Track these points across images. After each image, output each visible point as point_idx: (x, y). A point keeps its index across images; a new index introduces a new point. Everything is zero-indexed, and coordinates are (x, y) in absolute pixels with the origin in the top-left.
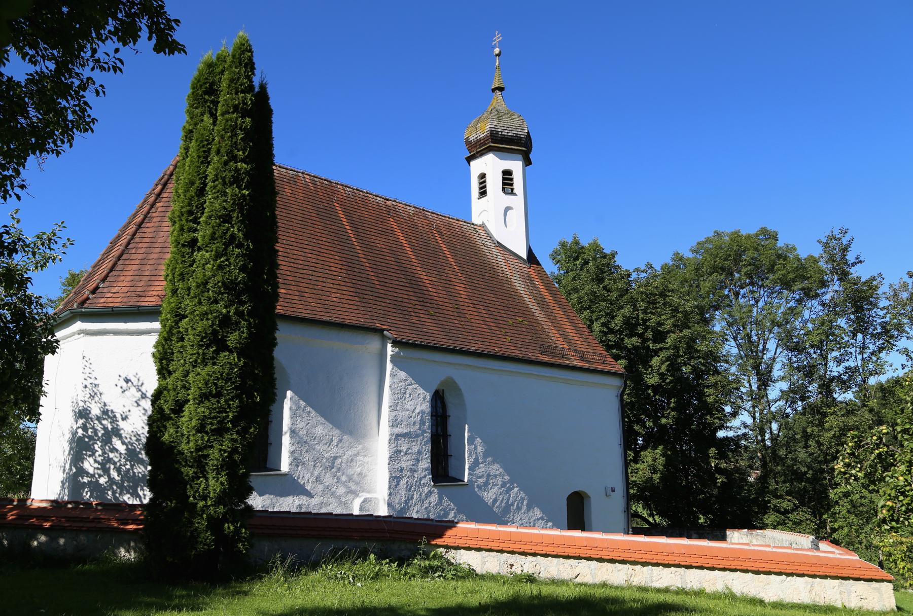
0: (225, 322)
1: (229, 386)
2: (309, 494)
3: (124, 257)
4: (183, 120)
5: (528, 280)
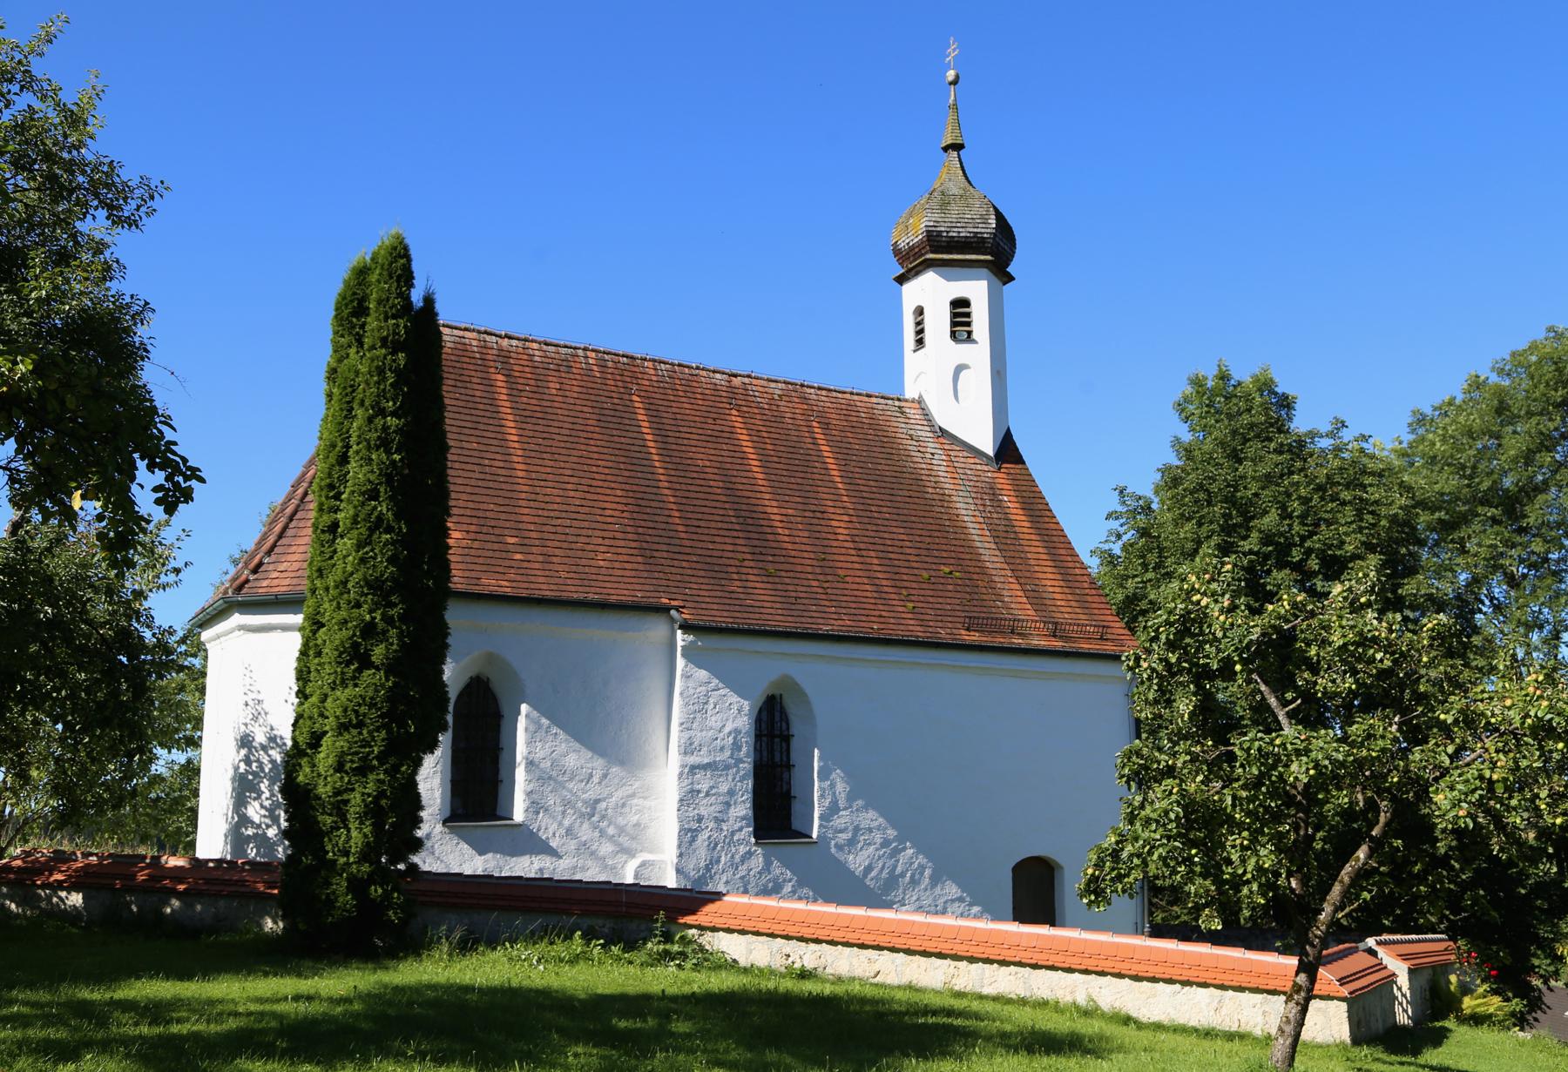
0: (368, 630)
1: (374, 714)
2: (554, 853)
3: (298, 516)
4: (324, 354)
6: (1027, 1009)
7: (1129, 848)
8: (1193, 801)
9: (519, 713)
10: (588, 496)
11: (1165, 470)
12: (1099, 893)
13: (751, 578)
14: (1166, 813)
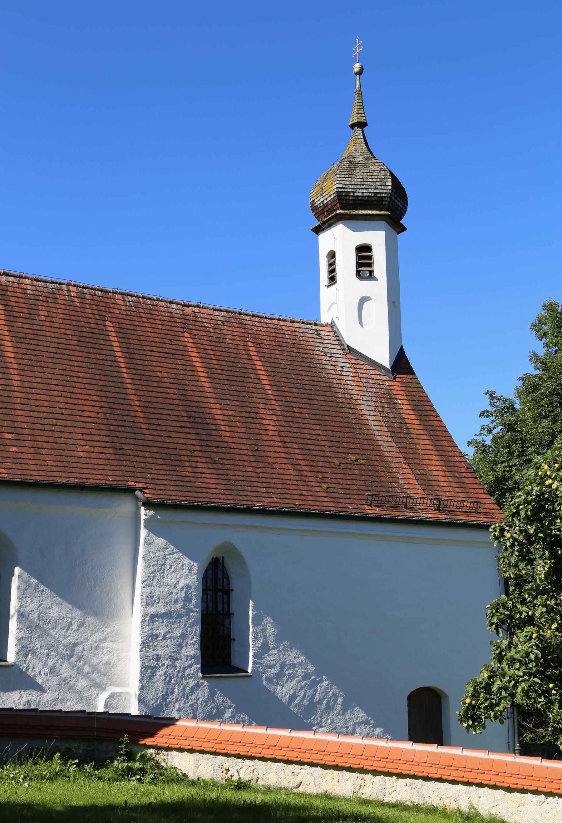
2: (40, 688)
5: (387, 399)
6: (421, 815)
7: (498, 683)
8: (549, 645)
9: (13, 574)
10: (71, 401)
11: (526, 379)
12: (475, 718)
13: (200, 465)
14: (528, 654)
